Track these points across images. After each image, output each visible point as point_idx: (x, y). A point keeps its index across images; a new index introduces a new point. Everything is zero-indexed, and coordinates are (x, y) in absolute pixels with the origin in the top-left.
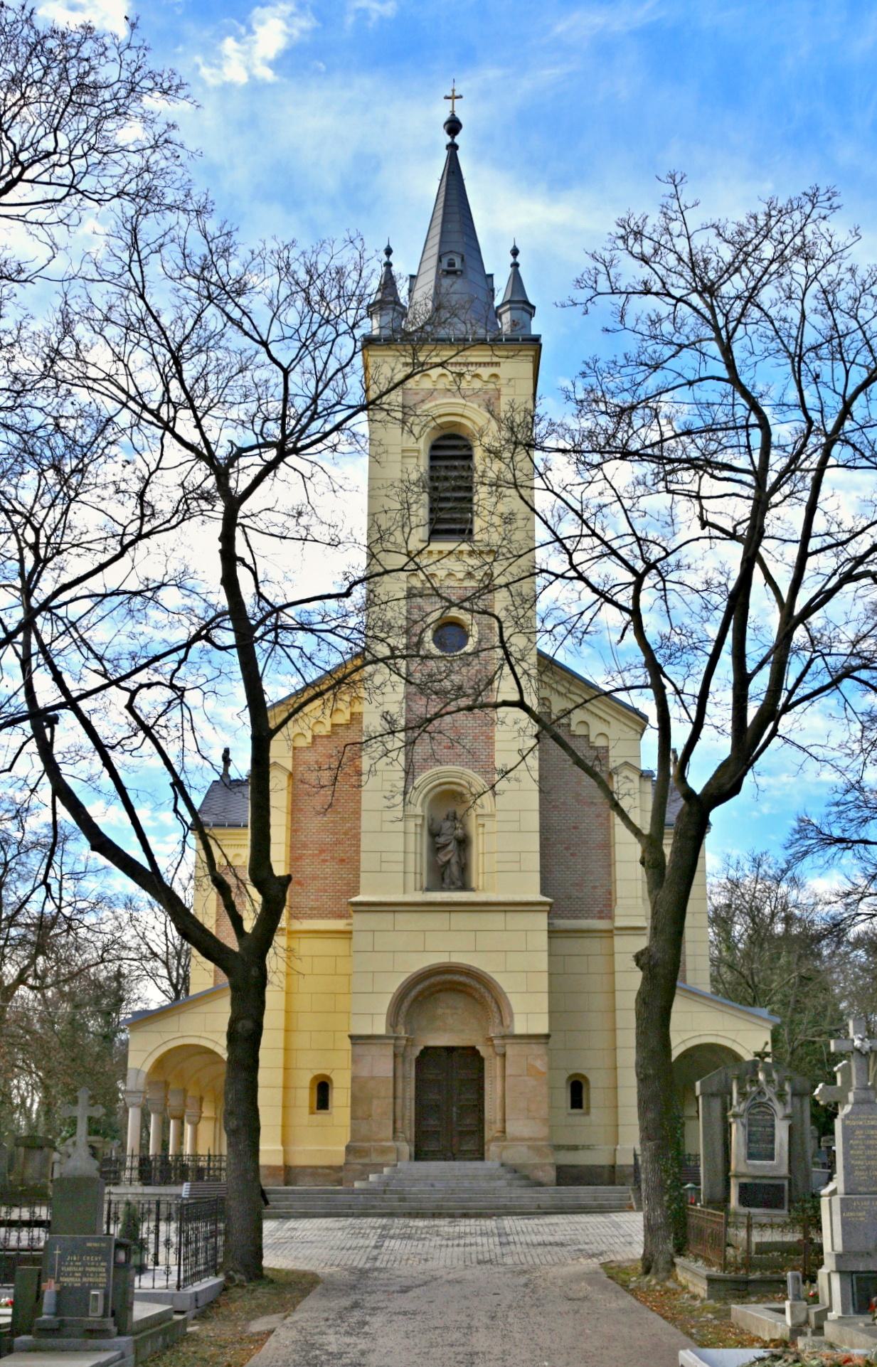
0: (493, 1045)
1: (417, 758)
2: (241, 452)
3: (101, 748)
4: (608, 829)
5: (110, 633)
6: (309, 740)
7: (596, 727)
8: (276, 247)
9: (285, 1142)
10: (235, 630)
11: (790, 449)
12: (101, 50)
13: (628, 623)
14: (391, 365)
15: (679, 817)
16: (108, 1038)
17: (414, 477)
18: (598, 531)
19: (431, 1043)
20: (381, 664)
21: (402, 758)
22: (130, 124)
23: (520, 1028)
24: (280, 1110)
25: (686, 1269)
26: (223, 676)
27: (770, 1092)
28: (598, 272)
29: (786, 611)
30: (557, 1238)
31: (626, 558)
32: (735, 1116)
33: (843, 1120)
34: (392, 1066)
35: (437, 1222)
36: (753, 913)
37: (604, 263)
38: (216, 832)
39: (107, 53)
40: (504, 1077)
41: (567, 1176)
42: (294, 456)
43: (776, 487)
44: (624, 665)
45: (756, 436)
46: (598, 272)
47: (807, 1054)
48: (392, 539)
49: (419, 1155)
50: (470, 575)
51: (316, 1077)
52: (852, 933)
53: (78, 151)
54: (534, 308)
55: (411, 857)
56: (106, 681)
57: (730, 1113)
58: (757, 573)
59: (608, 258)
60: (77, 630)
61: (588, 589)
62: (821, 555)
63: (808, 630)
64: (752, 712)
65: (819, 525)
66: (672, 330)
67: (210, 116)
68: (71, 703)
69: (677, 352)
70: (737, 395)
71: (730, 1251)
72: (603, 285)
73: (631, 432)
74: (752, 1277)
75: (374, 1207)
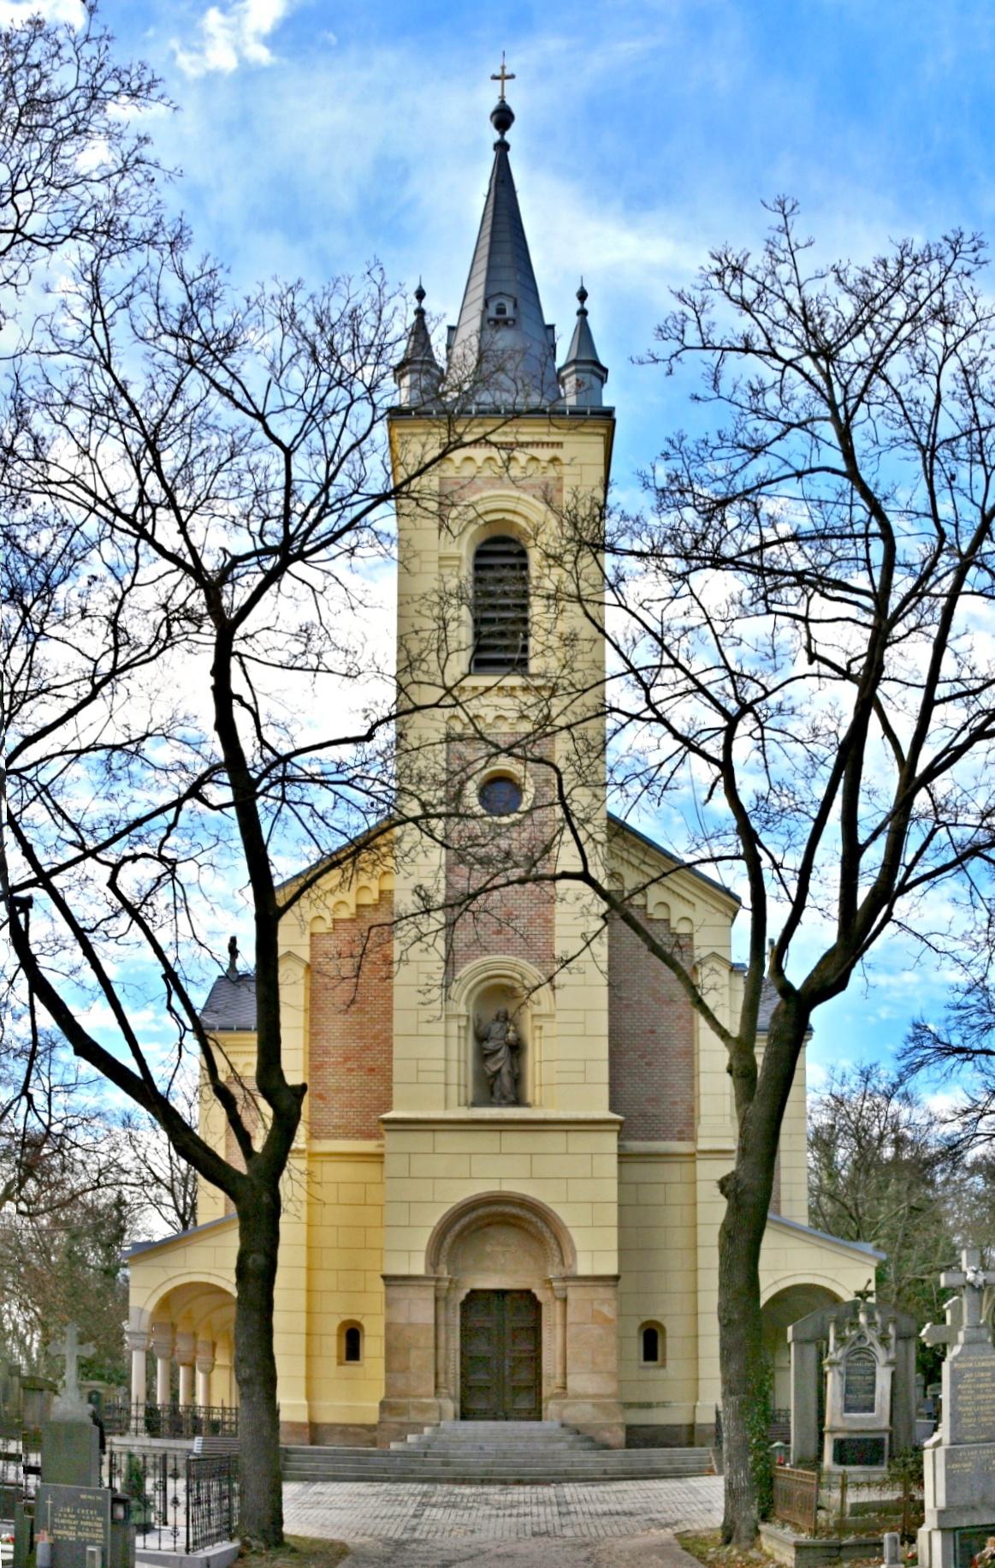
0: (552, 1288)
1: (458, 945)
2: (237, 560)
3: (80, 934)
4: (691, 1035)
5: (83, 793)
6: (329, 924)
7: (678, 910)
8: (277, 291)
9: (310, 1396)
10: (232, 785)
11: (918, 568)
12: (54, 49)
13: (717, 779)
14: (423, 443)
15: (774, 1017)
16: (109, 1273)
17: (452, 584)
18: (682, 661)
20: (411, 825)
21: (441, 945)
22: (92, 143)
23: (583, 1268)
24: (302, 1361)
25: (771, 1537)
26: (221, 845)
27: (872, 1336)
28: (686, 319)
29: (906, 770)
30: (626, 1507)
31: (716, 696)
32: (831, 1364)
33: (952, 1363)
35: (486, 1489)
36: (859, 1133)
37: (694, 306)
38: (220, 1036)
39: (61, 53)
40: (565, 1326)
41: (638, 1437)
42: (299, 563)
43: (897, 618)
44: (711, 830)
45: (877, 550)
46: (686, 319)
47: (916, 1294)
48: (424, 667)
49: (465, 1415)
50: (523, 717)
51: (344, 1324)
52: (970, 1156)
53: (22, 185)
54: (606, 371)
55: (454, 1066)
56: (81, 853)
57: (825, 1361)
58: (874, 718)
59: (698, 300)
60: (49, 796)
61: (670, 735)
62: (949, 704)
63: (931, 795)
64: (863, 893)
65: (948, 668)
66: (779, 404)
67: (191, 122)
68: (43, 879)
69: (784, 434)
70: (856, 494)
71: (822, 1514)
72: (692, 338)
73: (724, 532)
74: (845, 1542)
75: (412, 1471)
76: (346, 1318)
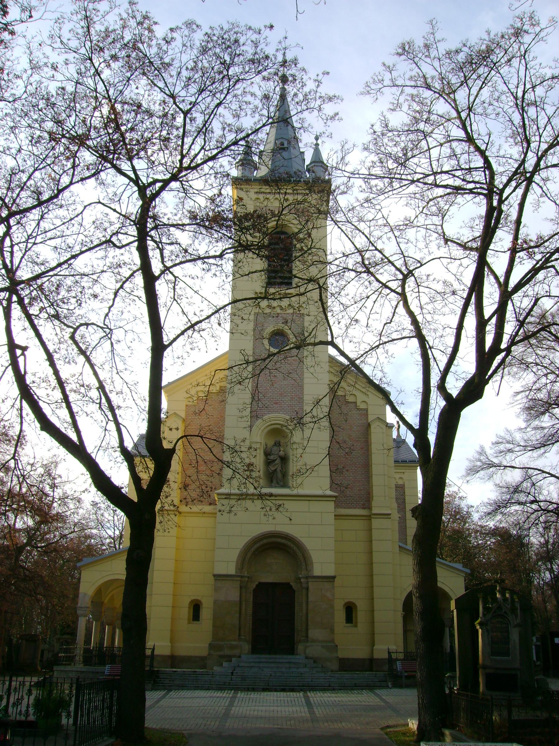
0: (301, 582)
19: (264, 580)
29: (503, 288)
34: (239, 594)
49: (255, 650)
51: (192, 601)
76: (193, 598)
